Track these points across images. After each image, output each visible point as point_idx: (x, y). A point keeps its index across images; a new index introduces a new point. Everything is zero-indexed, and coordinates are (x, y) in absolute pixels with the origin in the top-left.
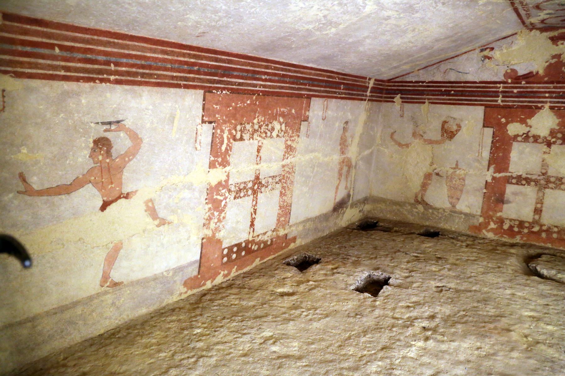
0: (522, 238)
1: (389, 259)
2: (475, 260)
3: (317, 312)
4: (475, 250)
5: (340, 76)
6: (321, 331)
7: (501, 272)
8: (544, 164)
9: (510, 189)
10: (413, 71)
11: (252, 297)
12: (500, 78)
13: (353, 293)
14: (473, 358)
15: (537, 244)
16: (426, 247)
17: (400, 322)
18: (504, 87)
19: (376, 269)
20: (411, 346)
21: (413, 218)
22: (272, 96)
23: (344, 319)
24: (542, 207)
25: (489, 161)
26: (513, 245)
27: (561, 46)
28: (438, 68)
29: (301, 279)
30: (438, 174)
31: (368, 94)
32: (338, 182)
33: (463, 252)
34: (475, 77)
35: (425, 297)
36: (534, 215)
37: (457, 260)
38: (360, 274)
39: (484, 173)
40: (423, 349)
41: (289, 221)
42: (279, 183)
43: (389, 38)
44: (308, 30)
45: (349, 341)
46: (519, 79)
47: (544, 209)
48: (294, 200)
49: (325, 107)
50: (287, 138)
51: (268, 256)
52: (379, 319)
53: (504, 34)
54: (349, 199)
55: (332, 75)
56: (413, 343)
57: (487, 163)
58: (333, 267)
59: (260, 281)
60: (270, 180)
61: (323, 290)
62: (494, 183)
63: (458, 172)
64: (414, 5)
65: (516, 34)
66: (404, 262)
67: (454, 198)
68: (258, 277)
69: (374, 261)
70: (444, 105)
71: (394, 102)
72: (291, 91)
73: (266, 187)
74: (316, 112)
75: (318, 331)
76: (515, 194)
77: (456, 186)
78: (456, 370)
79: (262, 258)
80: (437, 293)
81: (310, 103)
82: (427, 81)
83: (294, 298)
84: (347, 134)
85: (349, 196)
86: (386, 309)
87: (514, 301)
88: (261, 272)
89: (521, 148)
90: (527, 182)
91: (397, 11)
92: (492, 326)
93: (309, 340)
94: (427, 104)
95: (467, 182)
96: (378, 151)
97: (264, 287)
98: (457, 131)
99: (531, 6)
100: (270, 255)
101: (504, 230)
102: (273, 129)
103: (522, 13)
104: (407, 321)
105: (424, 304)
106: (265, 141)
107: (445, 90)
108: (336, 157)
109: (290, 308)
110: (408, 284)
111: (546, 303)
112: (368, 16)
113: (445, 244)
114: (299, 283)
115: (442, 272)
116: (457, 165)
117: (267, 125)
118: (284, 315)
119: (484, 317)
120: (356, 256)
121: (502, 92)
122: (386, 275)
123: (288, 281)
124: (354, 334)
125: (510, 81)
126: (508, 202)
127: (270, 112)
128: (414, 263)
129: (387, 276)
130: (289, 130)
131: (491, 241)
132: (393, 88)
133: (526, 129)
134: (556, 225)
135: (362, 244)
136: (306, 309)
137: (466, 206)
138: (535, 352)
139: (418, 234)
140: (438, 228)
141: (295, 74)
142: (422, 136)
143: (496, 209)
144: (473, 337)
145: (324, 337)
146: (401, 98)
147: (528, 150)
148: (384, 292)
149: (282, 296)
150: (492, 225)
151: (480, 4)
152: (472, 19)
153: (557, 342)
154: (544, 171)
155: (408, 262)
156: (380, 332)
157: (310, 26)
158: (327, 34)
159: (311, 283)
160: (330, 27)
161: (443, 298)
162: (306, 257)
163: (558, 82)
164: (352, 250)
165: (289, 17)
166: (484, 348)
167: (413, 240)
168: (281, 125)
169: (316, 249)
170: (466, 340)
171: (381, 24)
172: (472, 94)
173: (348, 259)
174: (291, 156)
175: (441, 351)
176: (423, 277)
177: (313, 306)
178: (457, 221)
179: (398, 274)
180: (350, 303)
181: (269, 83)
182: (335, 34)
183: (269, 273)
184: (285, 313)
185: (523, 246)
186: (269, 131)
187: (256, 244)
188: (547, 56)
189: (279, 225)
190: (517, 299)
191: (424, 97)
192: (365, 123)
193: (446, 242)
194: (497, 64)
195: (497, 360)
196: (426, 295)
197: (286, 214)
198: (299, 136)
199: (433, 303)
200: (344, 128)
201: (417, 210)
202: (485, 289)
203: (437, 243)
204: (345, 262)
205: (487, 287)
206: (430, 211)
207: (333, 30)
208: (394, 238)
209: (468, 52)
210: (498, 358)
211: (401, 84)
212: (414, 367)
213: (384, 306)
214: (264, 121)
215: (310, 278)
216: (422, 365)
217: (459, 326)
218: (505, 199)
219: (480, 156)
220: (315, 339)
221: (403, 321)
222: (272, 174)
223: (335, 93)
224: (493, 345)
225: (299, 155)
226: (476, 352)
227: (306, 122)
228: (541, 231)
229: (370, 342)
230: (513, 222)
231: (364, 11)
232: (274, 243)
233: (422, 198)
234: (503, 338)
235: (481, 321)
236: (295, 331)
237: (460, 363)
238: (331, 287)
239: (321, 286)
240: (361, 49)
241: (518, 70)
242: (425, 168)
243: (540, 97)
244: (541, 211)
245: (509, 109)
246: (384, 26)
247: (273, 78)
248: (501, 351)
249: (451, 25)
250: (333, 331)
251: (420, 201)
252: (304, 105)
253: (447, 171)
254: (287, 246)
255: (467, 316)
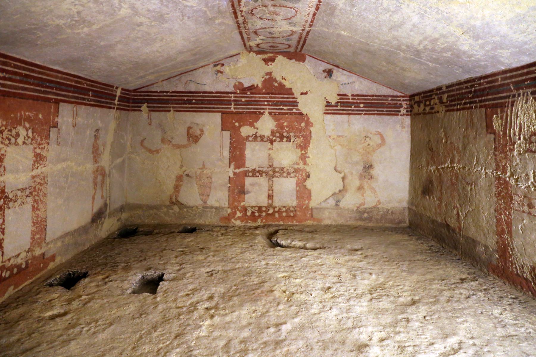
0: (262, 220)
1: (157, 258)
2: (232, 244)
3: (99, 323)
4: (229, 237)
5: (88, 83)
6: (109, 340)
7: (253, 249)
8: (270, 159)
9: (248, 181)
10: (157, 81)
11: (13, 331)
12: (231, 89)
13: (131, 297)
14: (253, 320)
15: (273, 223)
16: (188, 242)
17: (185, 309)
18: (235, 97)
19: (149, 269)
20: (201, 326)
21: (171, 219)
22: (14, 97)
23: (131, 322)
24: (273, 192)
25: (230, 159)
26: (256, 228)
27: (271, 66)
28: (179, 80)
29: (71, 297)
30: (188, 175)
31: (116, 102)
32: (94, 192)
33: (220, 240)
34: (211, 88)
35: (199, 283)
36: (268, 200)
37: (218, 247)
38: (134, 277)
39: (227, 170)
40: (211, 326)
41: (45, 238)
42: (29, 197)
43: (139, 45)
44: (58, 25)
45: (141, 341)
46: (245, 90)
47: (274, 194)
48: (49, 214)
49: (75, 113)
50: (36, 146)
51: (23, 282)
52: (164, 312)
53: (231, 53)
54: (107, 209)
55: (80, 80)
56: (202, 323)
57: (228, 161)
58: (103, 277)
59: (19, 311)
60: (19, 193)
61: (99, 300)
62: (235, 178)
63: (205, 172)
64: (165, 15)
65: (239, 54)
66: (173, 258)
67: (205, 195)
68: (16, 308)
69: (144, 263)
70: (187, 113)
71: (141, 111)
72: (37, 94)
73: (14, 202)
74: (65, 119)
75: (106, 341)
76: (253, 185)
77: (205, 184)
78: (243, 333)
79: (16, 286)
80: (209, 278)
81: (58, 108)
82: (170, 91)
83: (68, 317)
84: (98, 142)
85: (106, 205)
86: (168, 303)
87: (270, 268)
88: (19, 302)
89: (252, 147)
90: (260, 174)
91: (149, 18)
92: (259, 291)
93: (98, 354)
94: (172, 111)
95: (213, 180)
96: (130, 158)
97: (27, 316)
98: (201, 135)
99: (251, 31)
100: (27, 280)
101: (248, 216)
102: (18, 135)
103: (245, 36)
104: (191, 307)
105: (201, 289)
106: (8, 149)
107: (187, 99)
108: (90, 166)
109: (66, 328)
110: (182, 276)
111: (290, 264)
112: (123, 19)
113: (204, 236)
114: (70, 301)
115: (209, 259)
116: (204, 165)
117: (10, 130)
118: (62, 338)
119: (251, 287)
120: (124, 262)
121: (234, 101)
122: (159, 272)
123: (56, 302)
124: (144, 333)
125: (238, 92)
126: (248, 192)
127: (12, 115)
128: (181, 257)
129: (160, 273)
130: (36, 136)
131: (240, 227)
132: (139, 97)
133: (254, 131)
134: (284, 205)
135: (128, 250)
136: (86, 325)
137: (216, 201)
138: (293, 300)
139: (178, 232)
140: (194, 225)
141: (40, 76)
142: (171, 142)
143: (240, 199)
144: (248, 304)
145: (114, 345)
146: (148, 107)
147: (257, 148)
148: (162, 288)
149: (53, 319)
150: (239, 214)
151: (216, 23)
152: (209, 36)
153: (304, 289)
154: (271, 164)
155: (176, 257)
156: (168, 323)
157: (61, 21)
158: (79, 33)
159: (84, 297)
160: (82, 26)
161: (215, 280)
162: (69, 274)
163: (272, 94)
164: (119, 257)
165: (38, 6)
166: (259, 309)
167: (175, 237)
168: (27, 131)
169: (80, 264)
170: (244, 308)
171: (134, 29)
172: (210, 102)
173: (117, 266)
174: (42, 166)
175: (227, 323)
176: (194, 267)
177: (93, 319)
178: (209, 215)
179: (170, 269)
180: (131, 306)
181: (9, 83)
182: (87, 35)
183: (29, 299)
184: (61, 335)
185: (264, 227)
186: (13, 137)
187: (7, 269)
188: (263, 73)
189: (34, 243)
190: (271, 267)
191: (169, 105)
192: (115, 132)
193: (204, 234)
194: (228, 77)
195: (271, 315)
196: (201, 281)
197: (41, 230)
198: (48, 144)
199: (208, 286)
200: (95, 136)
201: (173, 211)
202: (246, 265)
203: (197, 236)
204: (114, 269)
205: (247, 263)
206: (185, 210)
207: (86, 30)
208: (156, 239)
209: (204, 66)
210: (271, 314)
211: (147, 94)
212: (209, 343)
213: (165, 300)
214: (6, 126)
215: (81, 293)
216: (214, 339)
217: (235, 299)
218: (246, 190)
219: (222, 156)
220: (105, 351)
221: (187, 308)
222: (20, 187)
223: (84, 99)
224: (264, 305)
225: (50, 164)
226: (254, 315)
227: (55, 129)
228: (274, 212)
229: (162, 335)
230: (254, 208)
231: (119, 13)
232: (29, 265)
233: (176, 199)
234: (270, 297)
235: (250, 290)
236: (79, 350)
237: (244, 327)
238: (107, 296)
239: (96, 297)
240: (112, 54)
241: (244, 83)
242: (176, 171)
243: (261, 105)
244: (273, 196)
245: (240, 115)
246: (136, 32)
247: (14, 77)
248: (271, 307)
249: (192, 39)
250: (122, 336)
251: (175, 202)
252: (52, 110)
253: (196, 172)
254: (45, 267)
255: (238, 289)
